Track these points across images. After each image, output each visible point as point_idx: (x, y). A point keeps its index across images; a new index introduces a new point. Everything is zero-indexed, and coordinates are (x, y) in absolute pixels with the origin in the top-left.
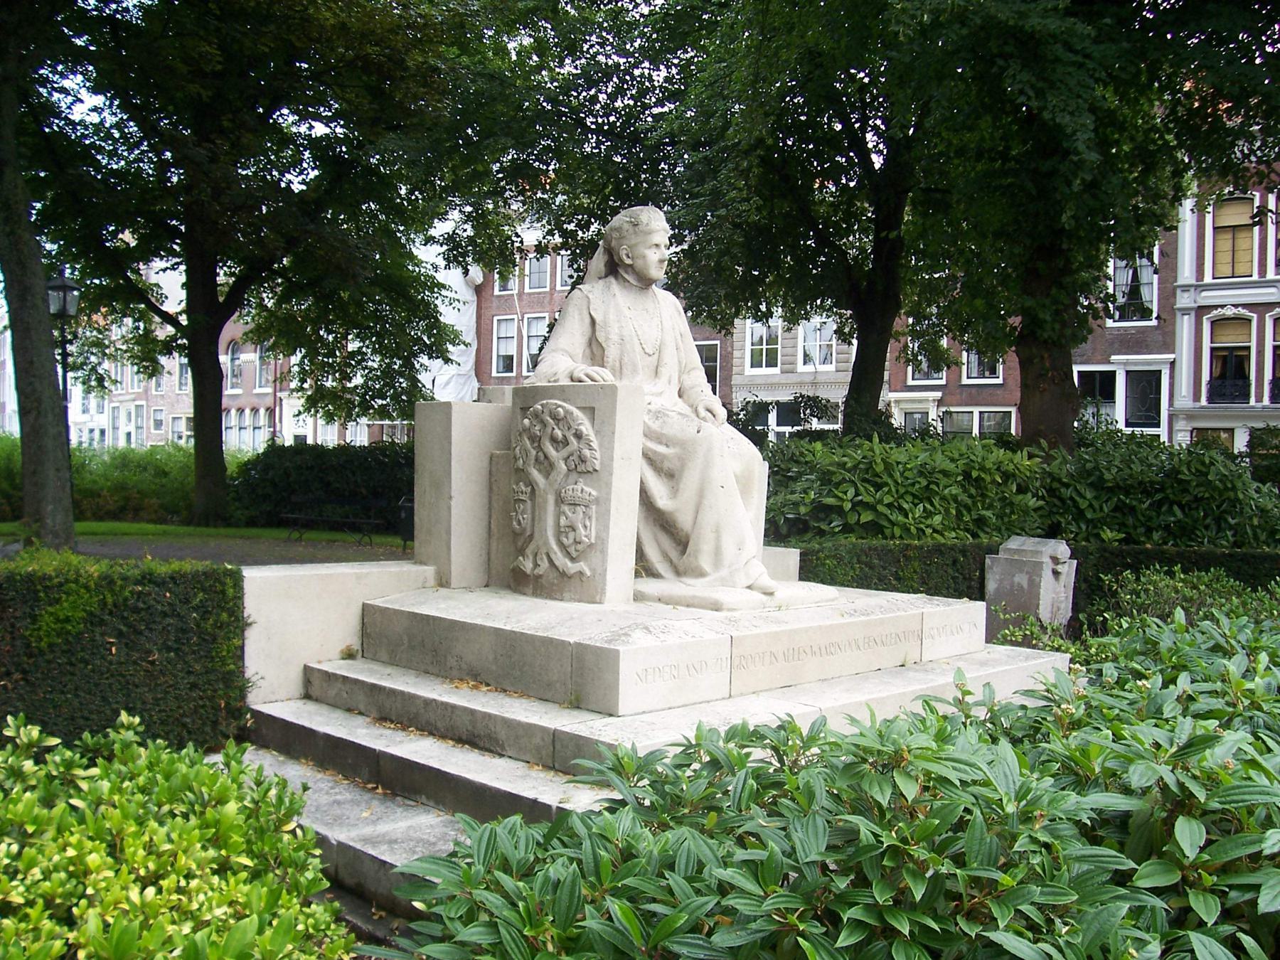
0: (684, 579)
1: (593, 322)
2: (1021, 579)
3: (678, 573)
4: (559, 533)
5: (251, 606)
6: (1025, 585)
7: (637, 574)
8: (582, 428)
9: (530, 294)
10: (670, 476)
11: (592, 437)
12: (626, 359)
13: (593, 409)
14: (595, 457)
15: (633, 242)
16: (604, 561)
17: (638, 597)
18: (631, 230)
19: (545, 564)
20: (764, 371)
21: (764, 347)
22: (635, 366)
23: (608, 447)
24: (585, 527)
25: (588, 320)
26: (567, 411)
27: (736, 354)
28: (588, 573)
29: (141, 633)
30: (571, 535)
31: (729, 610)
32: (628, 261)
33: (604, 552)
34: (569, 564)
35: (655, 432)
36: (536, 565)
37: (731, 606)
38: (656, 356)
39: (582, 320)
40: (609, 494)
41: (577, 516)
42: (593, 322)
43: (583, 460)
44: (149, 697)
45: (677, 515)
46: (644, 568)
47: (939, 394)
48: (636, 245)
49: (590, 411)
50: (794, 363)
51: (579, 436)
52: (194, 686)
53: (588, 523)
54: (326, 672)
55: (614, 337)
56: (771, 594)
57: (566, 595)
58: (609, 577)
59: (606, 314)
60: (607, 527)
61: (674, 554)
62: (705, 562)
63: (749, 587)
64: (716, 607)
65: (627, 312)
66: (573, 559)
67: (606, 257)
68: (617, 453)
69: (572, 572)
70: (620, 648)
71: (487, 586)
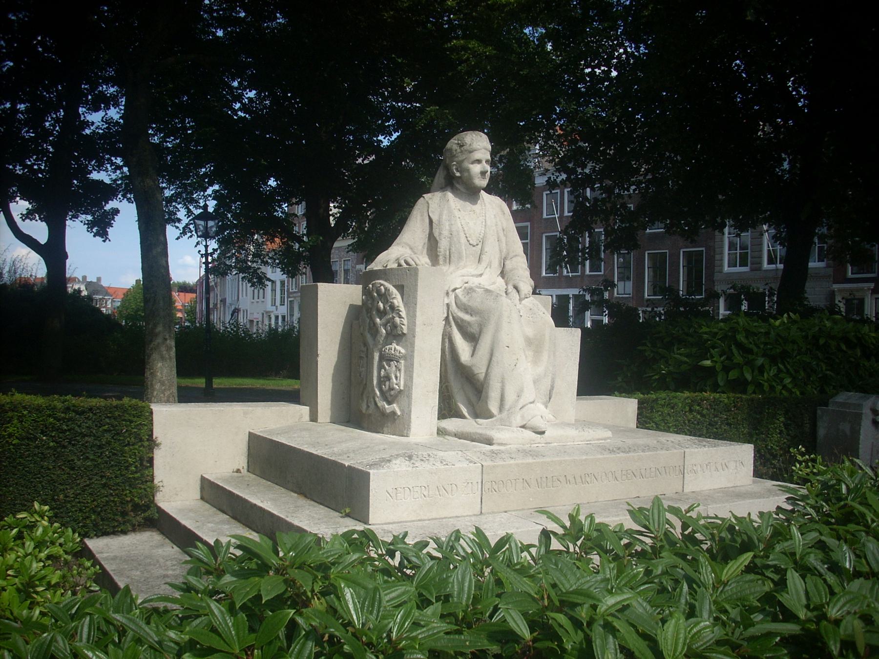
0: (480, 421)
1: (431, 221)
2: (846, 427)
3: (476, 415)
4: (381, 382)
5: (158, 432)
6: (848, 432)
7: (442, 416)
8: (395, 301)
9: (546, 219)
10: (473, 338)
11: (402, 308)
12: (453, 249)
13: (402, 286)
14: (403, 322)
15: (460, 159)
16: (410, 404)
17: (441, 432)
18: (459, 150)
19: (372, 406)
20: (739, 269)
21: (738, 251)
22: (460, 253)
23: (412, 316)
24: (396, 378)
25: (427, 221)
26: (386, 289)
27: (717, 257)
28: (399, 413)
29: (64, 447)
30: (387, 383)
31: (499, 444)
32: (458, 174)
33: (409, 397)
34: (387, 406)
35: (464, 305)
36: (368, 406)
37: (500, 441)
38: (479, 246)
39: (423, 220)
40: (413, 352)
41: (392, 369)
42: (431, 221)
43: (395, 326)
44: (71, 493)
45: (473, 368)
46: (447, 409)
47: (872, 285)
48: (463, 161)
49: (400, 288)
50: (761, 263)
51: (393, 308)
52: (104, 486)
53: (398, 375)
54: (210, 481)
55: (445, 233)
56: (543, 433)
57: (385, 429)
58: (413, 416)
59: (441, 215)
60: (411, 377)
61: (474, 399)
62: (493, 407)
63: (523, 427)
64: (489, 442)
65: (456, 213)
66: (389, 403)
67: (445, 172)
68: (419, 319)
69: (388, 411)
70: (371, 472)
71: (348, 422)
